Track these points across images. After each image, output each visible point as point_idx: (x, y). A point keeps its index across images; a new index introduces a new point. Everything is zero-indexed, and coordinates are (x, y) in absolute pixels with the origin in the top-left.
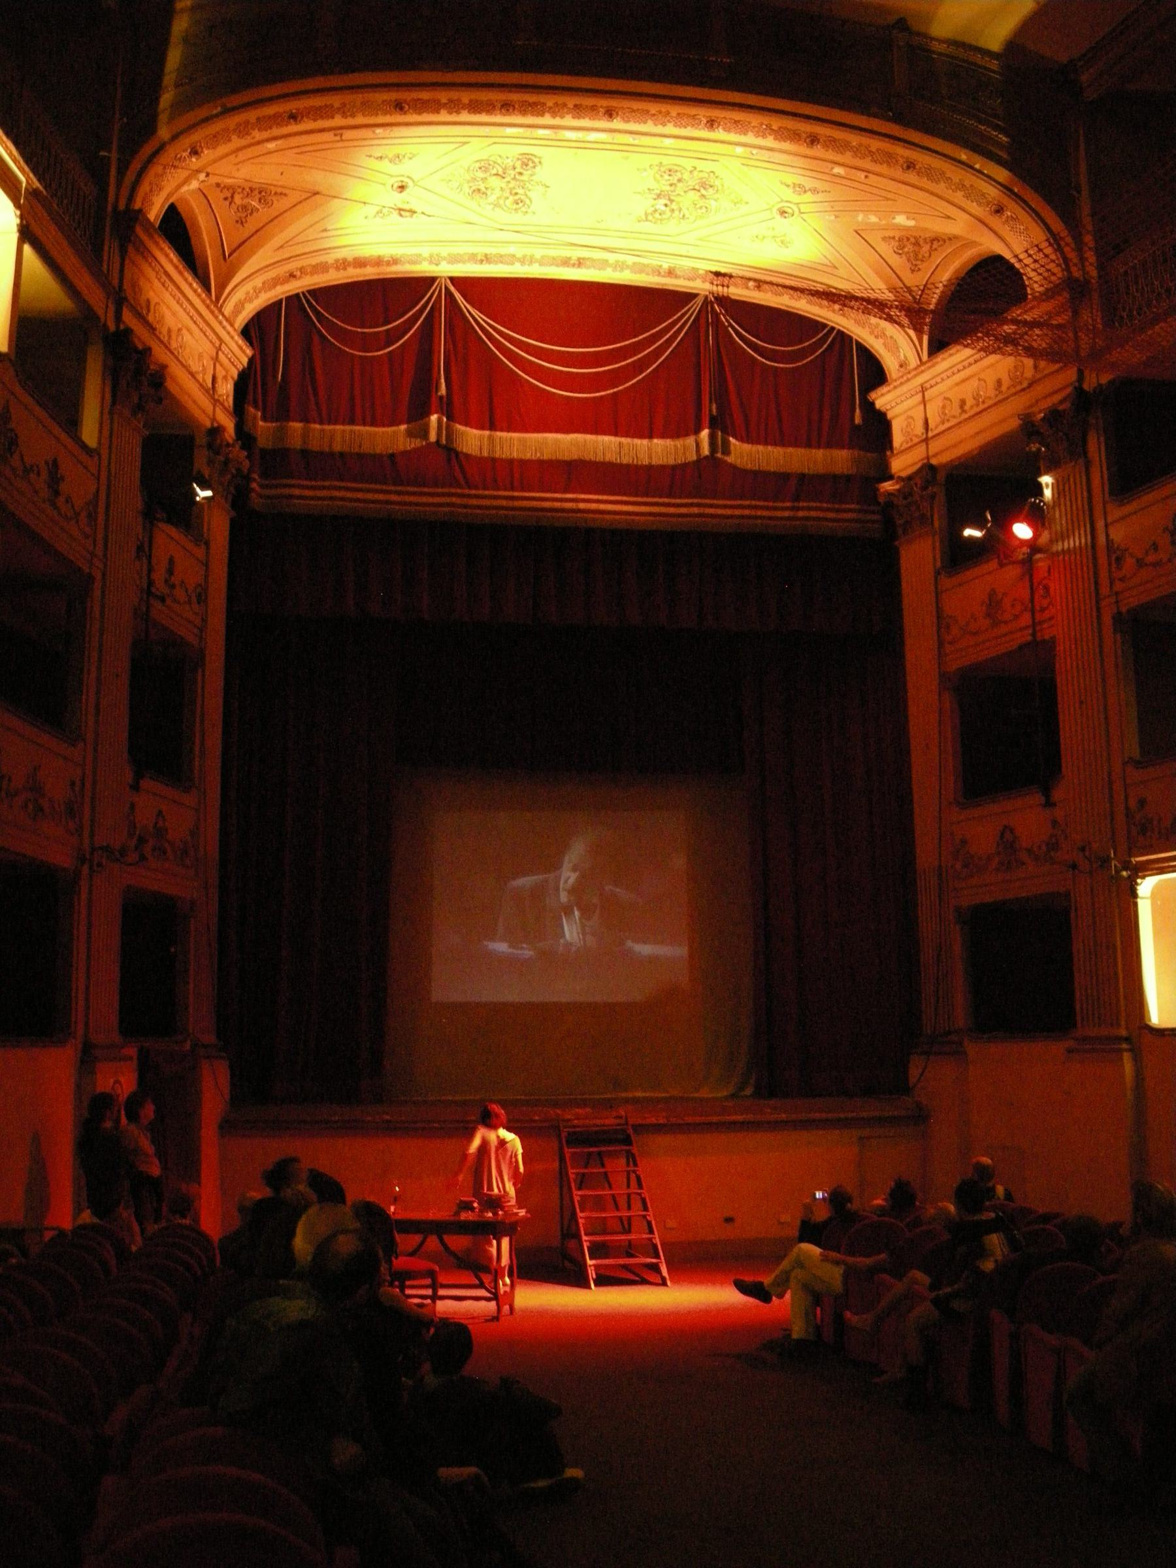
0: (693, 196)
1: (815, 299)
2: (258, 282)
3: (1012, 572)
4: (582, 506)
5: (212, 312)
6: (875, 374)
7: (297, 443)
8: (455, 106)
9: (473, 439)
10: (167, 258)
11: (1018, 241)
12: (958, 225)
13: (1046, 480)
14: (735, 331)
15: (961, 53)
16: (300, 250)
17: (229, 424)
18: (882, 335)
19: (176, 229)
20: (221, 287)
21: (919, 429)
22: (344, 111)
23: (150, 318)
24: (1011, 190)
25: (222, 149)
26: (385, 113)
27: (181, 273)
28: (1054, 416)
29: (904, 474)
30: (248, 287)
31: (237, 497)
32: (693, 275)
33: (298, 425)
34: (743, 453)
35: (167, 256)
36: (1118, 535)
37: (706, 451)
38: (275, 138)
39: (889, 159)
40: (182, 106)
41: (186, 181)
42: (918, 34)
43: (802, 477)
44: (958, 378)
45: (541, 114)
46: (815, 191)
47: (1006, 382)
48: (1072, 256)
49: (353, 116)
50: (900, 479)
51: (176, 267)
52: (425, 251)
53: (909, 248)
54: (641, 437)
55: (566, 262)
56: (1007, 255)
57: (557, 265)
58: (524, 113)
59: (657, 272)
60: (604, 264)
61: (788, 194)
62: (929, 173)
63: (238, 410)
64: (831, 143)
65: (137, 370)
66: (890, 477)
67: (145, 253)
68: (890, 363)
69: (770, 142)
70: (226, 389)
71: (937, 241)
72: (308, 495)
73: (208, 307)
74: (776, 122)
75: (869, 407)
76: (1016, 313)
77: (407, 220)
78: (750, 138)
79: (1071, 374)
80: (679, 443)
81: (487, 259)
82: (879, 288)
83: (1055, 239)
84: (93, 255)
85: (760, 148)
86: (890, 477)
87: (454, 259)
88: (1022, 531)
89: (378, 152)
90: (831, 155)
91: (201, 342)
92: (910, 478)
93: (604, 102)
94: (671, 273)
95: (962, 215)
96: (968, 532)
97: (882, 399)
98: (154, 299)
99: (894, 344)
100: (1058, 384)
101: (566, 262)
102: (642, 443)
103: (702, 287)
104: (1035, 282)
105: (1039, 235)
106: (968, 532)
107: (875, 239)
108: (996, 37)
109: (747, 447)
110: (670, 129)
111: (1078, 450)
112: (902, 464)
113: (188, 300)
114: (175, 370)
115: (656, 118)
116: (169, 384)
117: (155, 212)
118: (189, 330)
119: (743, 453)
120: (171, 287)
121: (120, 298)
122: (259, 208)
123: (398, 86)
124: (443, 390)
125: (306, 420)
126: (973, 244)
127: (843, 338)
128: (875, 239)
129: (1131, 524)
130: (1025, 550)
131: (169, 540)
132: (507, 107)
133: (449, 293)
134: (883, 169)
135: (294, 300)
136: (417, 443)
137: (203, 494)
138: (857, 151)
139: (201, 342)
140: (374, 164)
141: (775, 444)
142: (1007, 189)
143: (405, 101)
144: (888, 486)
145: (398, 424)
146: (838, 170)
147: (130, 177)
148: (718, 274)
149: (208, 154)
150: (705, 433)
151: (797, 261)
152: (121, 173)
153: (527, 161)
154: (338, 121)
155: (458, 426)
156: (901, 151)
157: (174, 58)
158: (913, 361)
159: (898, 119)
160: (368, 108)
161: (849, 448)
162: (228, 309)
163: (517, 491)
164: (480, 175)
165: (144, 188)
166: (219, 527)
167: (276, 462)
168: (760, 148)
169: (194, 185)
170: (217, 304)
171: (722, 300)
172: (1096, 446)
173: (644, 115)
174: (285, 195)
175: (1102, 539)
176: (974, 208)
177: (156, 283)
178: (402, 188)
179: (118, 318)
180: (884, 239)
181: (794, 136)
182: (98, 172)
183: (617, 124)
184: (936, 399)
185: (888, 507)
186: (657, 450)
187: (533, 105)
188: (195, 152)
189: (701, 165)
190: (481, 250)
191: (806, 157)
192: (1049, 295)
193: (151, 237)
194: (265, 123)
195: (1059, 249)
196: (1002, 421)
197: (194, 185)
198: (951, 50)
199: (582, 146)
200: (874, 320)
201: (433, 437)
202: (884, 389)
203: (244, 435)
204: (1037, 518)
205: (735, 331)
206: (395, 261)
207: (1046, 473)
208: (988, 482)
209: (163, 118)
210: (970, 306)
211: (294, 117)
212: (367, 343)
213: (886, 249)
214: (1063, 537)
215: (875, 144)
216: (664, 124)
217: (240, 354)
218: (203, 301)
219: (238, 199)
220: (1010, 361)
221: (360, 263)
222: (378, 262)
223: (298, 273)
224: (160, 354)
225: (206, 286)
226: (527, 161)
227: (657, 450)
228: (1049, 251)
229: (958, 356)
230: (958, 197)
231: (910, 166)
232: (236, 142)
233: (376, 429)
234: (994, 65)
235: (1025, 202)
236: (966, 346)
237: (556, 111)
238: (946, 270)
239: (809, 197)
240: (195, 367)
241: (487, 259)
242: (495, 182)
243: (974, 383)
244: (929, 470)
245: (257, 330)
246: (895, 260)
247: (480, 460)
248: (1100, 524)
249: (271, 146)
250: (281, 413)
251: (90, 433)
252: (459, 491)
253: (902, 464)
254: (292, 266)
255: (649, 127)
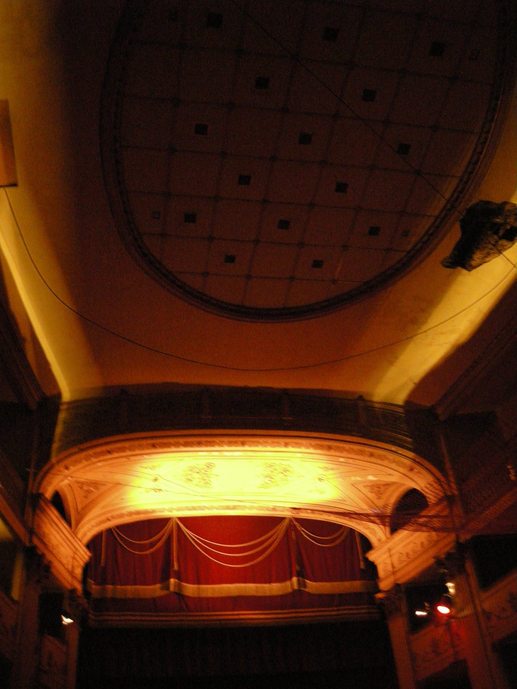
0: (281, 475)
1: (336, 515)
2: (93, 523)
3: (441, 630)
4: (243, 617)
5: (72, 536)
6: (367, 545)
7: (109, 595)
8: (177, 445)
9: (190, 589)
10: (53, 514)
11: (422, 482)
12: (395, 478)
13: (450, 585)
14: (304, 532)
15: (387, 407)
16: (111, 508)
17: (79, 587)
18: (368, 528)
19: (58, 501)
20: (78, 523)
21: (390, 568)
22: (130, 449)
23: (45, 540)
24: (415, 461)
25: (79, 466)
26: (148, 448)
27: (59, 520)
28: (449, 556)
29: (386, 589)
30: (89, 526)
31: (81, 620)
32: (284, 509)
33: (110, 587)
34: (313, 586)
35: (53, 512)
36: (486, 606)
37: (296, 587)
38: (100, 461)
39: (362, 453)
40: (63, 448)
41: (62, 481)
42: (369, 401)
43: (340, 595)
44: (404, 543)
45: (213, 446)
46: (332, 469)
47: (426, 543)
48: (446, 487)
49: (134, 450)
50: (385, 591)
51: (57, 517)
52: (166, 506)
53: (376, 489)
54: (265, 582)
55: (228, 508)
56: (418, 488)
57: (224, 509)
58: (206, 446)
59: (268, 509)
60: (244, 508)
61: (322, 472)
62: (380, 457)
63: (84, 581)
64: (338, 449)
65: (38, 562)
66: (380, 591)
67: (43, 511)
68: (373, 540)
69: (311, 450)
70: (79, 571)
71: (387, 485)
72: (115, 618)
73: (70, 534)
74: (314, 442)
75: (366, 560)
76: (424, 513)
77: (158, 493)
78: (303, 450)
79: (452, 537)
80: (283, 585)
81: (194, 508)
82: (365, 509)
83: (438, 480)
84: (21, 514)
85: (307, 453)
86: (380, 591)
87: (179, 509)
88: (443, 610)
89: (145, 465)
90: (338, 454)
91: (68, 549)
92: (388, 591)
93: (241, 439)
94: (274, 509)
95: (397, 473)
96: (418, 613)
97: (372, 556)
98: (47, 531)
99: (375, 532)
100: (447, 543)
101: (228, 508)
102: (266, 586)
103: (287, 514)
104: (432, 498)
105: (430, 478)
106: (418, 613)
107: (360, 487)
108: (400, 399)
109: (314, 584)
110: (269, 448)
111: (462, 570)
112: (385, 585)
113: (63, 532)
114: (56, 564)
115: (265, 444)
116: (53, 570)
117: (49, 494)
118: (62, 545)
119: (313, 586)
120: (54, 526)
121: (33, 531)
122: (94, 491)
123: (152, 438)
124: (176, 567)
125: (113, 584)
126: (402, 485)
127: (352, 531)
128: (360, 487)
129: (492, 600)
130: (445, 618)
131: (51, 643)
132: (199, 444)
133: (178, 525)
134: (361, 457)
135: (109, 531)
136: (165, 592)
137: (67, 621)
138: (349, 451)
139: (68, 549)
140: (144, 470)
141: (326, 581)
142: (414, 460)
143: (157, 444)
144: (380, 595)
145: (155, 584)
146: (342, 460)
147: (39, 478)
148: (295, 509)
149: (72, 468)
150: (295, 579)
151: (328, 500)
152: (34, 481)
153: (209, 466)
154: (128, 453)
155: (185, 584)
156: (368, 449)
157: (59, 429)
158: (383, 538)
159: (364, 436)
160: (141, 447)
161: (359, 580)
162: (80, 535)
163: (211, 611)
164: (190, 473)
165: (45, 483)
166: (74, 637)
167: (101, 604)
168: (307, 453)
169: (66, 482)
170: (75, 534)
171: (298, 520)
172: (470, 567)
173: (258, 444)
174: (105, 485)
175: (479, 609)
176: (402, 470)
177: (49, 526)
178: (156, 480)
179: (31, 541)
180: (365, 487)
181: (321, 447)
182: (25, 478)
183: (247, 448)
184: (395, 554)
185: (381, 605)
186: (274, 588)
187: (209, 442)
188: (67, 468)
189: (283, 462)
190: (190, 505)
191: (328, 455)
192: (437, 504)
193: (46, 504)
194: (96, 455)
195: (441, 485)
196: (426, 561)
197: (66, 482)
198: (383, 406)
199: (233, 458)
200: (364, 522)
201: (172, 588)
202: (372, 552)
203: (87, 593)
204: (448, 603)
205: (304, 532)
206: (153, 511)
207: (450, 581)
208: (424, 589)
209: (54, 454)
210: (405, 511)
211: (109, 452)
212: (142, 548)
213: (366, 491)
214: (462, 610)
215: (356, 447)
216: (266, 446)
217: (85, 555)
218: (68, 531)
219: (85, 488)
220: (425, 534)
221: (138, 513)
222: (146, 512)
223: (110, 518)
224: (49, 557)
225: (69, 524)
226: (209, 466)
227: (274, 588)
228: (435, 485)
229: (402, 534)
230: (393, 466)
231: (372, 455)
232: (85, 463)
233: (147, 587)
234: (401, 410)
235: (422, 465)
236: (405, 529)
237: (220, 444)
238: (392, 498)
239: (331, 472)
240: (64, 561)
241: (194, 508)
242: (196, 475)
243: (412, 545)
244: (397, 586)
245: (93, 545)
246: (371, 495)
247: (194, 599)
248: (477, 602)
249: (99, 464)
250: (103, 582)
251: (16, 593)
252: (184, 614)
253: (385, 585)
254: (109, 515)
255: (260, 448)
